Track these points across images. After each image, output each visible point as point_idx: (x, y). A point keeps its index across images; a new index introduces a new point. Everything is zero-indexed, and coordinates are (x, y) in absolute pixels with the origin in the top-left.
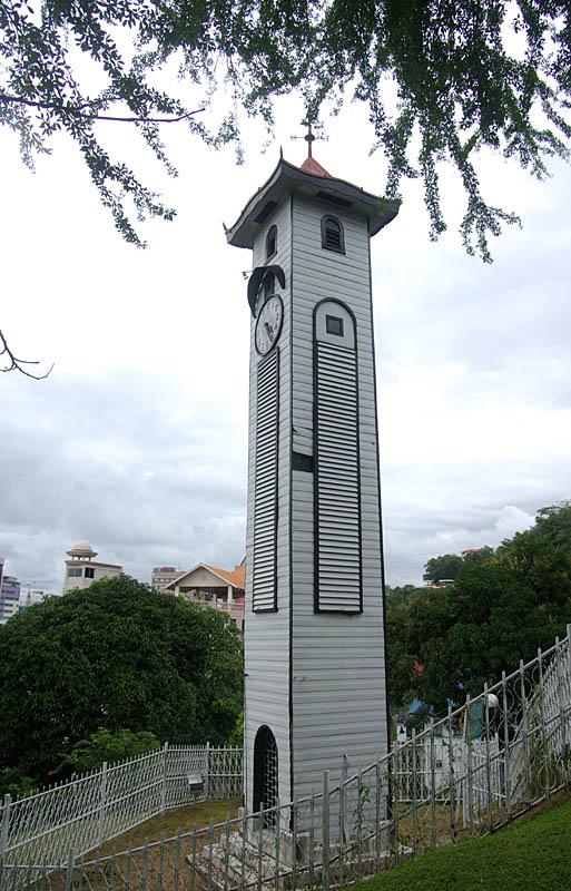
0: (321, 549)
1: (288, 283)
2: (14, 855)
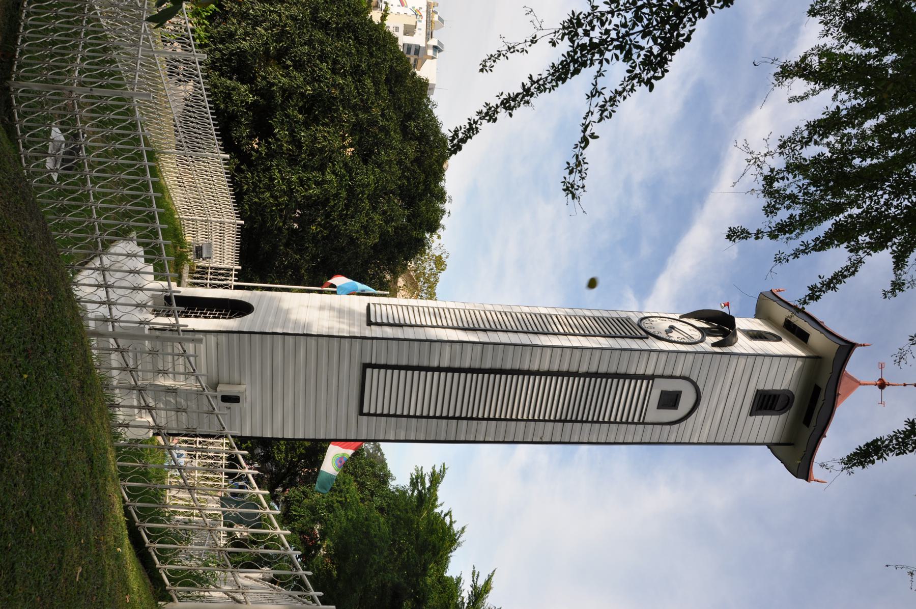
1: (717, 350)
2: (154, 71)
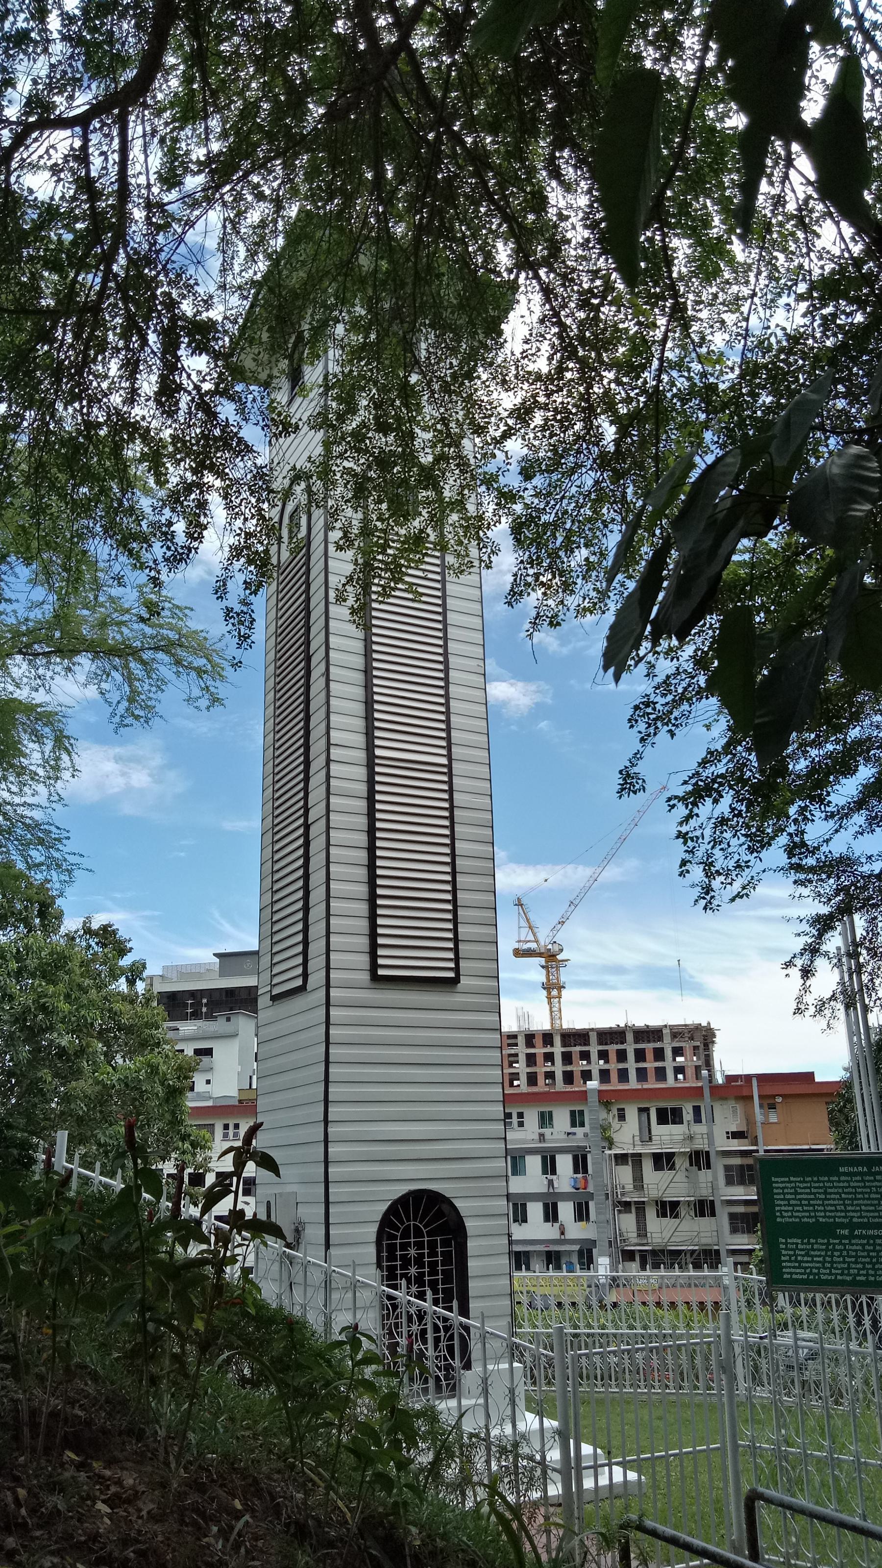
0: (379, 844)
